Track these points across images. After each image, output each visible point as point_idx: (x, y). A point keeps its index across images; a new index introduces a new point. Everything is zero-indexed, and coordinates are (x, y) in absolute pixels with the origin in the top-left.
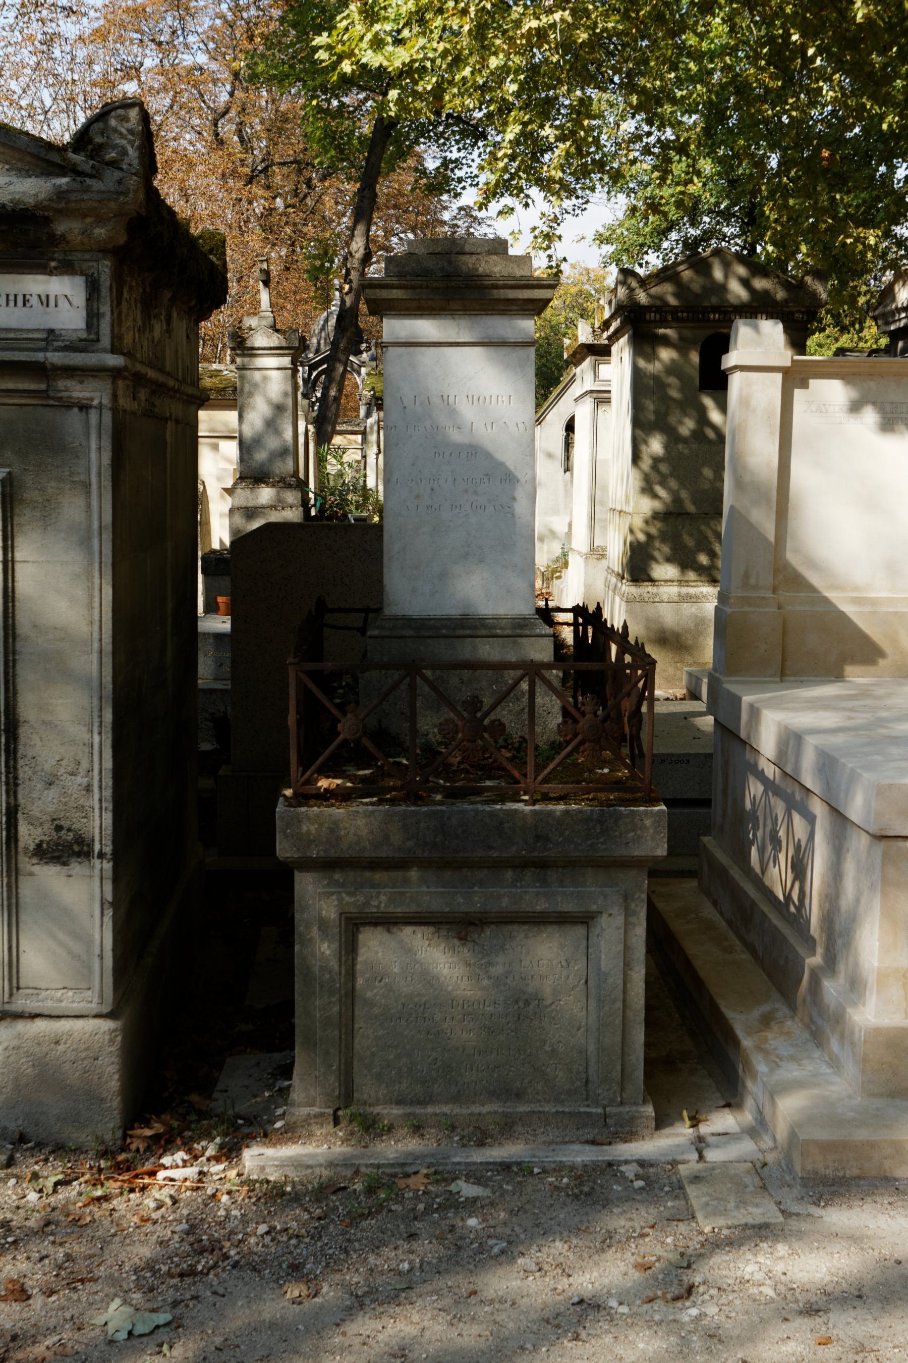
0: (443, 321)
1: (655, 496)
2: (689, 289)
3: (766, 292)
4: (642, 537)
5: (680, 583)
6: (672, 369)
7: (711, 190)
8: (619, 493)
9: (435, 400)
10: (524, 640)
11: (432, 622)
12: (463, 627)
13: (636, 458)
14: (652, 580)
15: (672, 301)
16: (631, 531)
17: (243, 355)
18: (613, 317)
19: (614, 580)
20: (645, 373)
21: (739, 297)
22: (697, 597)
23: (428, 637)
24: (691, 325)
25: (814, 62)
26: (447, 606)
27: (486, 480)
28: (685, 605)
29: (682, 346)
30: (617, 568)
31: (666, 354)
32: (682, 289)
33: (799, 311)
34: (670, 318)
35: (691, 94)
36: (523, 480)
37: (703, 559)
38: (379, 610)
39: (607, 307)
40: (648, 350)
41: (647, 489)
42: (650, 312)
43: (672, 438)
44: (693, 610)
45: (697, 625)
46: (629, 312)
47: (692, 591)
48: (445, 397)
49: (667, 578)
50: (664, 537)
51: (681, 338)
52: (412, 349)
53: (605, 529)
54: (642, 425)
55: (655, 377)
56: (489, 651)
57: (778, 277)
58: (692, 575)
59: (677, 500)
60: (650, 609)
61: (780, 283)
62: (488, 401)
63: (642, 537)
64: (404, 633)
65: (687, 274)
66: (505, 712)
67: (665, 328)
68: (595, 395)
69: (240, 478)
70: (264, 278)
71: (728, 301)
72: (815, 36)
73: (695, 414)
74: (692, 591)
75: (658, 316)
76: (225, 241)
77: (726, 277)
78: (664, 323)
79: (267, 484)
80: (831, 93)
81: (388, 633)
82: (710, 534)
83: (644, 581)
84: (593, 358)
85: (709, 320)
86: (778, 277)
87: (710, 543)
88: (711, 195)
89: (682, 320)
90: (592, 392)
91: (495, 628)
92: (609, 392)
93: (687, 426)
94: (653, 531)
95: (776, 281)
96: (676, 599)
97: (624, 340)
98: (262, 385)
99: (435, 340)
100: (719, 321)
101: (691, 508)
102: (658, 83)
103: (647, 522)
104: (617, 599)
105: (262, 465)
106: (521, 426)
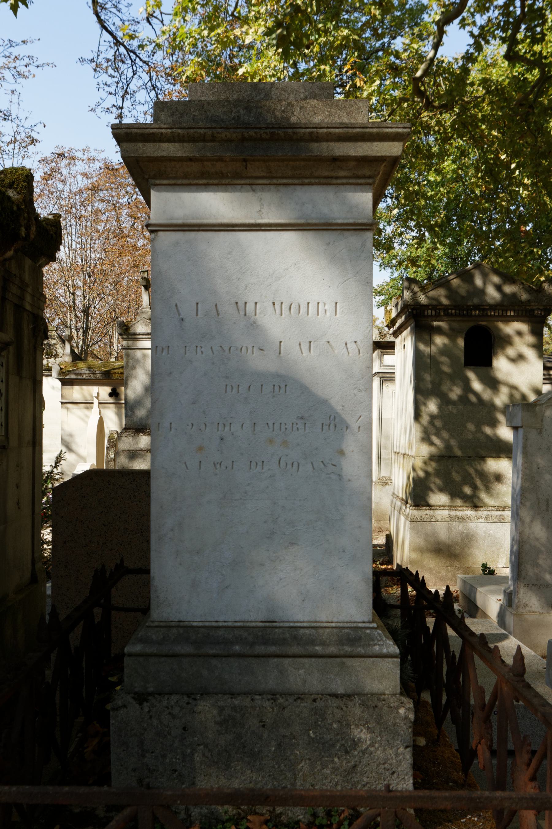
0: (238, 194)
1: (431, 443)
2: (457, 292)
3: (514, 295)
4: (421, 474)
5: (451, 507)
6: (444, 351)
7: (442, 263)
8: (403, 441)
9: (227, 309)
10: (356, 662)
11: (221, 632)
12: (266, 642)
13: (417, 416)
14: (429, 506)
15: (445, 301)
16: (414, 469)
17: (128, 339)
18: (398, 316)
19: (399, 503)
20: (424, 355)
21: (494, 298)
22: (463, 518)
23: (215, 656)
24: (458, 319)
25: (515, 173)
26: (242, 608)
27: (300, 426)
28: (454, 524)
29: (451, 335)
30: (401, 494)
31: (440, 340)
32: (452, 293)
33: (538, 309)
34: (442, 314)
35: (437, 194)
36: (354, 426)
37: (467, 490)
38: (146, 610)
39: (394, 310)
40: (427, 337)
41: (426, 439)
42: (428, 309)
43: (444, 401)
44: (460, 528)
45: (463, 539)
46: (412, 309)
47: (459, 513)
48: (241, 304)
49: (441, 504)
50: (437, 473)
51: (451, 329)
52: (193, 234)
53: (390, 465)
54: (421, 392)
55: (431, 357)
56: (303, 676)
57: (523, 283)
58: (459, 502)
59: (448, 447)
60: (428, 527)
61: (524, 288)
62: (303, 310)
63: (421, 474)
64: (178, 649)
65: (456, 282)
66: (327, 771)
67: (439, 321)
68: (381, 375)
69: (125, 429)
70: (145, 284)
71: (486, 301)
72: (517, 156)
73: (461, 384)
74: (459, 513)
75: (434, 313)
76: (32, 177)
77: (485, 284)
78: (437, 318)
79: (144, 433)
80: (525, 192)
81: (153, 649)
82: (472, 471)
83: (423, 506)
84: (380, 351)
85: (471, 316)
86: (523, 283)
87: (473, 478)
88: (442, 266)
89: (451, 315)
90: (379, 373)
91: (312, 642)
92: (394, 373)
93: (455, 393)
94: (430, 469)
95: (521, 286)
96: (447, 519)
97: (406, 332)
98: (142, 361)
99: (226, 221)
100: (479, 316)
101: (458, 452)
102: (416, 187)
103: (425, 463)
104: (402, 519)
105: (141, 419)
106: (351, 346)
